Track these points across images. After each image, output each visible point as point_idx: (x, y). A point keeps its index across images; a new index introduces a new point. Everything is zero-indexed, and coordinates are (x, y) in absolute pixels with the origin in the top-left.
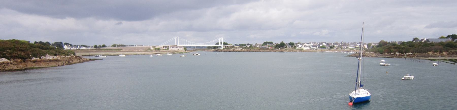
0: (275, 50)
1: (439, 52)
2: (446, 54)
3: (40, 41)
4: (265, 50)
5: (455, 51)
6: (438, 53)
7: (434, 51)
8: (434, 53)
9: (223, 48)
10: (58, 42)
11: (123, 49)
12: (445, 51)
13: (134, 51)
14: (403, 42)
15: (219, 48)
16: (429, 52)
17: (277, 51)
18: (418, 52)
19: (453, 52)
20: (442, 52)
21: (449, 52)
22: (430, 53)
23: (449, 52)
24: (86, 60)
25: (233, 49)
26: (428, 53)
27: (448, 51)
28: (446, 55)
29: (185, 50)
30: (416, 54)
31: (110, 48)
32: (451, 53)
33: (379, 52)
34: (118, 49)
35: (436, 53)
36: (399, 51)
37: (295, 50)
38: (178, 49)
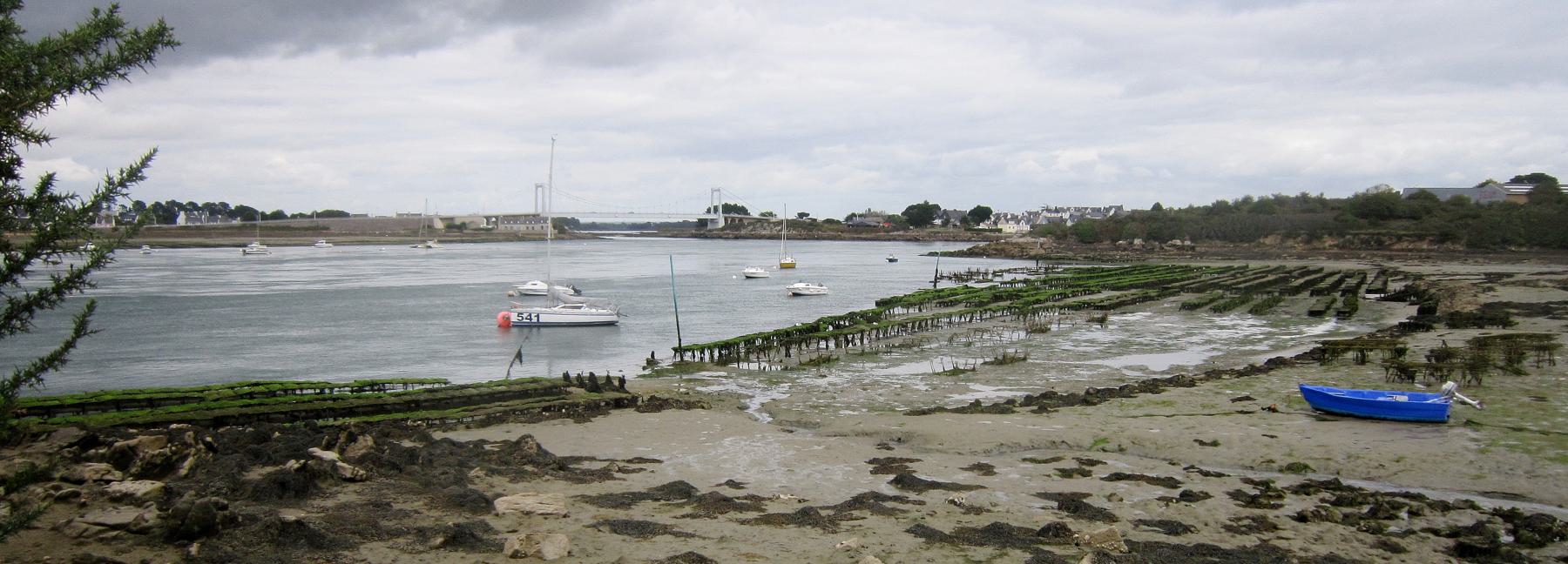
0: (895, 233)
1: (1304, 236)
2: (1335, 246)
3: (169, 200)
4: (860, 233)
5: (1374, 234)
6: (1302, 242)
7: (1283, 231)
8: (1283, 241)
9: (721, 224)
10: (214, 204)
11: (332, 228)
12: (1330, 234)
13: (370, 235)
14: (1256, 199)
15: (710, 226)
16: (1266, 237)
17: (900, 235)
18: (1218, 238)
19: (1362, 236)
20: (1319, 238)
21: (1348, 237)
22: (1268, 241)
23: (1348, 237)
24: (687, 533)
25: (752, 230)
26: (1261, 241)
27: (1342, 235)
28: (1336, 250)
29: (559, 233)
30: (1536, 249)
31: (288, 224)
32: (1356, 241)
33: (1077, 235)
34: (313, 225)
35: (1290, 243)
36: (1149, 234)
37: (969, 234)
38: (530, 226)
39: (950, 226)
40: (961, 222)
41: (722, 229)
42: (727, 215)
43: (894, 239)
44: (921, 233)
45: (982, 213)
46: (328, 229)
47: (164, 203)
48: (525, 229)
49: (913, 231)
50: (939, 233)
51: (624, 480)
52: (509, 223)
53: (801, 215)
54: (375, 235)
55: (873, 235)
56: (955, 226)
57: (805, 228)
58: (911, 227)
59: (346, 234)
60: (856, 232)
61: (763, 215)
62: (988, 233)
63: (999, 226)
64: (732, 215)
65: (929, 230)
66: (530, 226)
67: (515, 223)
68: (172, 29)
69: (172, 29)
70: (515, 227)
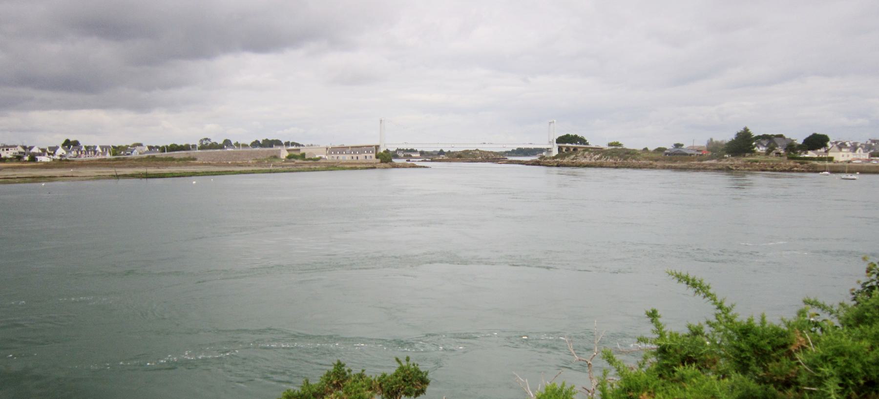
4: (675, 161)
17: (711, 165)
25: (573, 159)
37: (792, 163)
38: (355, 156)
39: (773, 154)
40: (786, 150)
41: (556, 157)
42: (561, 145)
43: (705, 169)
44: (736, 162)
45: (817, 141)
46: (194, 159)
47: (169, 146)
48: (350, 158)
49: (729, 161)
50: (757, 162)
51: (415, 277)
52: (355, 153)
53: (677, 146)
54: (228, 165)
55: (685, 164)
56: (778, 154)
57: (620, 157)
58: (727, 156)
59: (205, 164)
60: (670, 160)
61: (610, 145)
62: (815, 163)
63: (830, 155)
64: (567, 145)
65: (748, 158)
66: (355, 156)
67: (341, 153)
68: (673, 278)
69: (673, 278)
70: (341, 157)
